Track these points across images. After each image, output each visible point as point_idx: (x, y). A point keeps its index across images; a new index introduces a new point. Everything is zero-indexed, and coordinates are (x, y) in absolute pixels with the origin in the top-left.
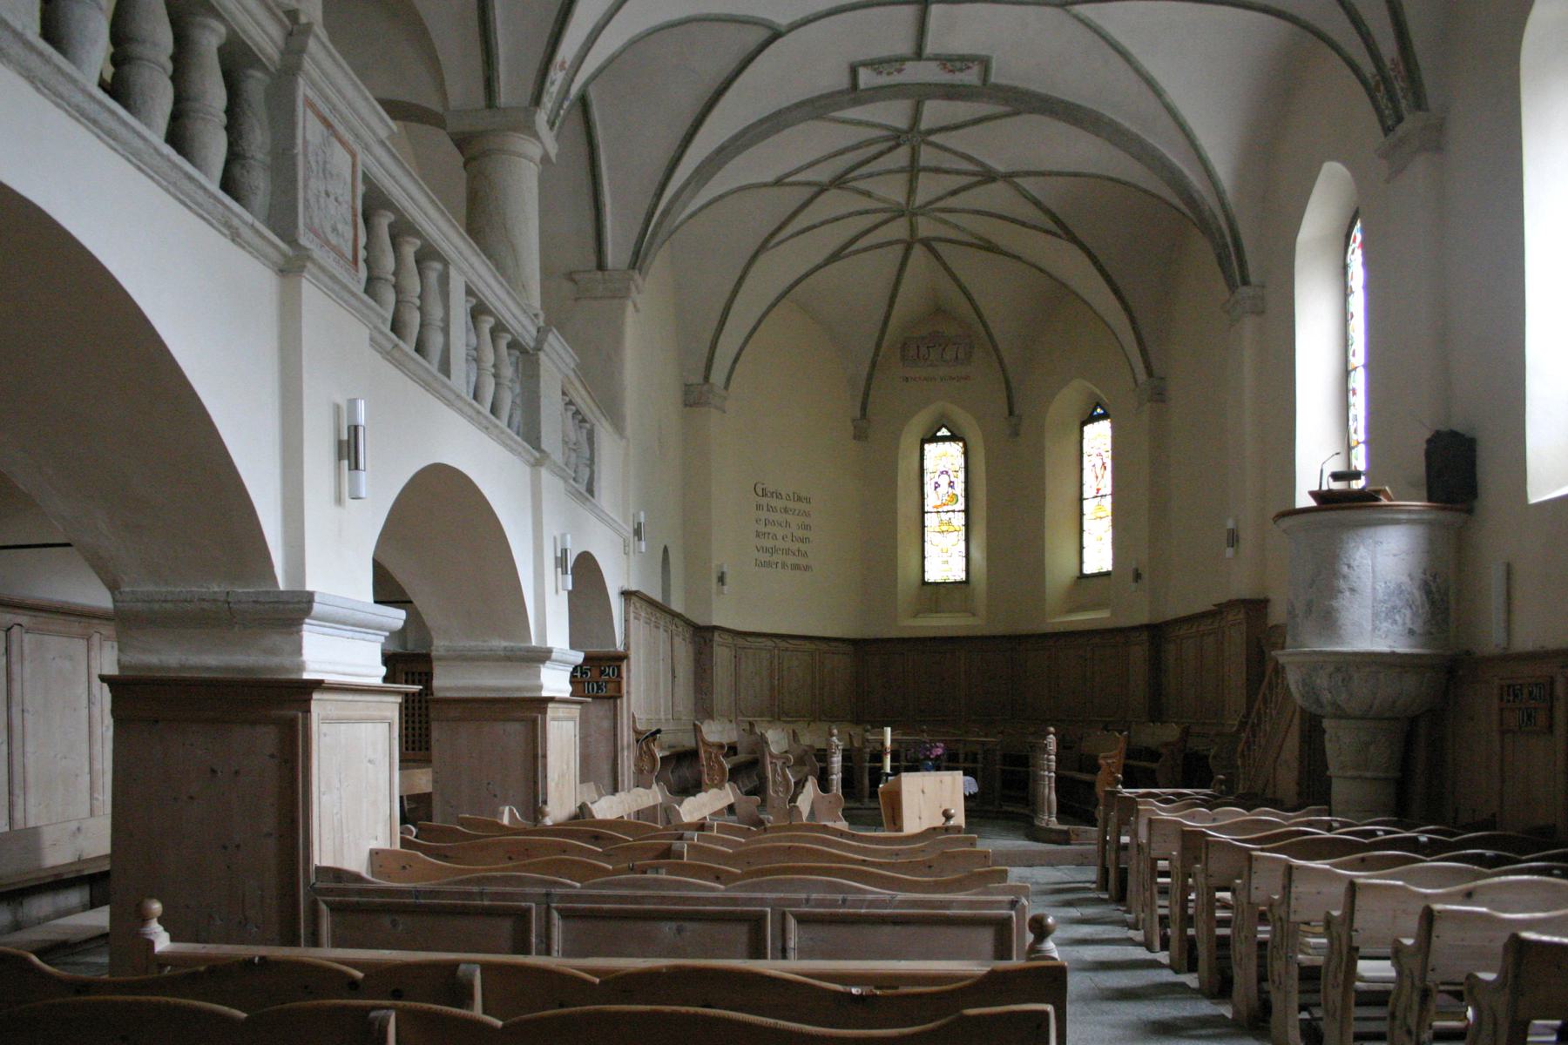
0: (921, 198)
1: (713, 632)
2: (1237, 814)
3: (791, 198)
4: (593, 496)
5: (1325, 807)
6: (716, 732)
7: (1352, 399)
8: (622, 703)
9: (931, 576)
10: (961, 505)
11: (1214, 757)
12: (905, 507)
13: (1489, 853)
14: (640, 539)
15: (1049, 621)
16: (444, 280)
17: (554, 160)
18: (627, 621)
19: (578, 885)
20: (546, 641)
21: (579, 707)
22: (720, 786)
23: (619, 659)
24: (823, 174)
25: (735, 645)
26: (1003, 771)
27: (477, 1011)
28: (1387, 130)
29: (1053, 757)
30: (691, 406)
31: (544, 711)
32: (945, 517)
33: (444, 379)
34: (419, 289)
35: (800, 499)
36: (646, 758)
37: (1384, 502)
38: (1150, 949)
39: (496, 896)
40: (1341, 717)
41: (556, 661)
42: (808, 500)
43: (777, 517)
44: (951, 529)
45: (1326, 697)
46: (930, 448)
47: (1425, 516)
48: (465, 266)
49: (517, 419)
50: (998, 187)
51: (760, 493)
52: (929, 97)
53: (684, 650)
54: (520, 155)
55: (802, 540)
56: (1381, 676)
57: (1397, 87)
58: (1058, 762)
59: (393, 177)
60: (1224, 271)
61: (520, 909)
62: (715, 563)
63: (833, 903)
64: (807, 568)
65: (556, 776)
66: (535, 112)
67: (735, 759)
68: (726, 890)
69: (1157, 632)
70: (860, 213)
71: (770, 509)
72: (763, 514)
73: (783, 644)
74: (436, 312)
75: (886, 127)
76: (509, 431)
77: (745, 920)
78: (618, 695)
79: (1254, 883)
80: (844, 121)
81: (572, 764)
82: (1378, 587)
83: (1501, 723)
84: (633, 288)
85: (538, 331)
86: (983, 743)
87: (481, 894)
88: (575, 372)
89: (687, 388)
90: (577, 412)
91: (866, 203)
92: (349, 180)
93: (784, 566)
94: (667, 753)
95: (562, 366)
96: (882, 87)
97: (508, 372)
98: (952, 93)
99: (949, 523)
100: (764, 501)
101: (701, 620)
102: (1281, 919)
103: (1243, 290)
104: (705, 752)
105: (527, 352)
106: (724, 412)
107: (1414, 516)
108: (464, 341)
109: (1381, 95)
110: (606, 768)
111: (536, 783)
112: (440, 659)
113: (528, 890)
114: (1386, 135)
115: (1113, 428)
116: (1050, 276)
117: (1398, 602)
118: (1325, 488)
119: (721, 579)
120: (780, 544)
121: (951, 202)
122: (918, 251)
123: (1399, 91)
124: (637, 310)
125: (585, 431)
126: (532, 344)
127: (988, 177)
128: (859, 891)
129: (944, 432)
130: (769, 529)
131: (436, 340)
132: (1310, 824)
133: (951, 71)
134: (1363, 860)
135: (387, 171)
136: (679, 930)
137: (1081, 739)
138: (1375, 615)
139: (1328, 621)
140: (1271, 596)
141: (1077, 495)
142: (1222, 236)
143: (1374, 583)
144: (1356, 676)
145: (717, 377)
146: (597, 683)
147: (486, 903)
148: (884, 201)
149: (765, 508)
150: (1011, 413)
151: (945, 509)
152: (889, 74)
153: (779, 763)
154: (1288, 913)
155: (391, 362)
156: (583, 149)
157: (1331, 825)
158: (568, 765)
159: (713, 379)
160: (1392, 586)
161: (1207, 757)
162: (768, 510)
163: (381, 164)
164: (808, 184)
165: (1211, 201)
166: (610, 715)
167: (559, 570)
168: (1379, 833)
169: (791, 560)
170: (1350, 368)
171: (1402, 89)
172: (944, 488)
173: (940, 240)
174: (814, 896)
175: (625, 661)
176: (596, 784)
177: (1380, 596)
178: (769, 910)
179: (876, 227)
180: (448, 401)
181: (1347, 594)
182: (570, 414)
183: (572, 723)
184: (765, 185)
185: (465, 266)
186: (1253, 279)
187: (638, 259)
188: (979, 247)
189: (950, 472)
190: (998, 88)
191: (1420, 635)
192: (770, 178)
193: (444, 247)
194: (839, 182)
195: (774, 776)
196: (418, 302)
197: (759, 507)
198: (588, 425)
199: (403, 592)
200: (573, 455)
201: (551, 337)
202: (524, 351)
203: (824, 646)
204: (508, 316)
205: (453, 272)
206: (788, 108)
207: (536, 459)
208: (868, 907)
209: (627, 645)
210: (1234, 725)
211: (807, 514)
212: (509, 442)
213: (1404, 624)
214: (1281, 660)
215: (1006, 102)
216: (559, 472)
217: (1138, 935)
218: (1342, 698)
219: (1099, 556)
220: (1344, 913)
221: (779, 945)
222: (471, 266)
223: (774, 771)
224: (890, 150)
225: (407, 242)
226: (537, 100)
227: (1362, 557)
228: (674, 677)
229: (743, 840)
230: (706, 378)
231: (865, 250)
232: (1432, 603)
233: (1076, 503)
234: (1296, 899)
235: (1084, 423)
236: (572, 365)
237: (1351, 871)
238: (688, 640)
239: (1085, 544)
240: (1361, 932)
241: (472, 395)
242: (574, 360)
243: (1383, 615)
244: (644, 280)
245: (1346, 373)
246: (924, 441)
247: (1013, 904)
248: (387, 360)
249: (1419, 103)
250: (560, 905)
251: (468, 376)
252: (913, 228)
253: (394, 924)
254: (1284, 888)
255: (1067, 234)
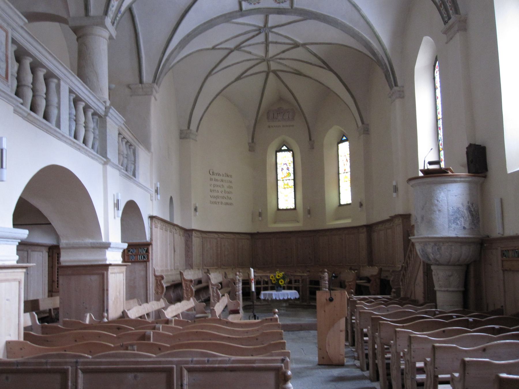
0: (271, 54)
1: (192, 232)
2: (396, 308)
3: (219, 55)
4: (135, 177)
5: (434, 304)
6: (190, 275)
7: (439, 131)
8: (149, 264)
9: (281, 207)
10: (292, 177)
11: (392, 281)
12: (270, 179)
13: (497, 327)
14: (158, 194)
15: (327, 224)
16: (58, 86)
17: (115, 37)
18: (151, 229)
19: (90, 357)
20: (109, 240)
21: (125, 267)
22: (188, 299)
23: (146, 246)
24: (231, 45)
25: (202, 237)
26: (310, 287)
27: (279, 322)
28: (445, 23)
29: (327, 282)
30: (183, 139)
31: (107, 270)
32: (286, 182)
33: (58, 130)
34: (45, 90)
35: (228, 176)
36: (160, 287)
37: (450, 173)
38: (362, 370)
39: (53, 363)
40: (438, 265)
41: (114, 248)
42: (231, 176)
43: (218, 183)
44: (288, 187)
45: (431, 256)
46: (279, 154)
47: (467, 179)
48: (68, 81)
49: (97, 145)
50: (300, 49)
51: (211, 174)
52: (271, 13)
53: (179, 239)
54: (99, 36)
55: (229, 193)
56: (453, 247)
57: (448, 5)
58: (329, 284)
59: (30, 43)
60: (388, 81)
61: (64, 369)
62: (193, 202)
63: (203, 362)
64: (231, 204)
65: (113, 299)
66: (105, 18)
67: (200, 286)
68: (156, 357)
69: (369, 228)
70: (248, 60)
71: (216, 180)
72: (213, 182)
73: (221, 236)
74: (54, 99)
75: (254, 26)
76: (92, 151)
77: (165, 371)
78: (148, 260)
79: (398, 343)
80: (238, 23)
81: (122, 293)
82: (450, 209)
83: (503, 266)
84: (154, 91)
85: (106, 108)
86: (301, 276)
87: (46, 363)
88: (124, 125)
89: (181, 132)
90: (127, 142)
91: (249, 57)
92: (4, 43)
93: (222, 203)
94: (169, 285)
95: (118, 122)
96: (251, 10)
97: (91, 125)
98: (280, 11)
99: (288, 184)
100: (213, 177)
101: (187, 227)
102: (408, 361)
103: (395, 88)
104: (185, 283)
105: (101, 117)
106: (196, 141)
107: (462, 179)
108: (68, 112)
109: (442, 8)
110: (142, 292)
111: (103, 302)
112: (64, 248)
113: (68, 360)
114: (445, 25)
115: (349, 143)
116: (323, 84)
117: (458, 215)
118: (426, 168)
119: (196, 210)
120: (220, 194)
121: (283, 56)
122: (271, 76)
123: (449, 7)
124: (156, 99)
125: (132, 150)
126: (103, 114)
127: (296, 45)
128: (215, 356)
129: (284, 148)
130: (216, 188)
131: (54, 112)
132: (426, 313)
133: (278, 3)
134: (444, 331)
135: (27, 40)
136: (135, 377)
137: (340, 273)
138: (449, 221)
139: (430, 223)
140: (411, 213)
141: (337, 171)
142: (386, 67)
143: (448, 207)
144: (443, 248)
145: (193, 127)
146: (143, 255)
147: (49, 367)
148: (256, 55)
149: (214, 180)
150: (310, 139)
151: (286, 178)
152: (254, 4)
153: (215, 288)
154: (411, 358)
155: (28, 121)
156: (133, 35)
157: (435, 313)
158: (120, 293)
159: (191, 128)
160: (455, 209)
161: (389, 281)
162: (215, 180)
163: (23, 37)
164: (226, 49)
165: (381, 53)
166: (145, 269)
167: (116, 208)
168: (454, 317)
169: (224, 201)
170: (438, 118)
171: (450, 6)
172: (285, 170)
173: (278, 70)
174: (195, 359)
175: (151, 246)
176: (137, 300)
177: (451, 213)
178: (175, 366)
179: (254, 66)
180: (59, 138)
181: (437, 212)
182: (124, 143)
183: (122, 275)
184: (208, 49)
185: (68, 81)
186: (399, 84)
187: (156, 79)
188: (296, 74)
189: (287, 164)
190: (296, 9)
191: (468, 229)
192: (210, 46)
193: (57, 72)
194: (238, 48)
195: (213, 294)
196: (45, 96)
197: (211, 179)
198: (133, 147)
199: (48, 221)
200: (125, 160)
201: (111, 111)
202: (100, 116)
203: (237, 236)
204: (90, 102)
205: (62, 83)
206: (215, 19)
207: (105, 162)
208: (219, 364)
209: (151, 239)
210: (399, 267)
211: (231, 182)
212: (91, 155)
213: (461, 225)
214: (413, 241)
215: (300, 14)
216: (114, 166)
217: (357, 363)
218: (438, 257)
219: (346, 198)
220: (431, 360)
221: (180, 383)
222: (71, 81)
223: (213, 291)
224: (257, 35)
225: (40, 70)
226: (106, 13)
227: (442, 197)
228: (175, 251)
229: (181, 328)
230: (189, 128)
231: (251, 75)
232: (472, 215)
233: (337, 175)
234: (414, 352)
235: (339, 143)
236: (122, 122)
237: (437, 338)
238: (181, 235)
239: (279, 197)
240: (438, 368)
241: (73, 135)
242: (123, 120)
243: (452, 221)
244: (159, 88)
245: (437, 120)
246: (277, 152)
247: (283, 361)
248: (26, 120)
249: (457, 11)
250: (82, 367)
251: (70, 126)
252: (269, 66)
253: (7, 378)
254: (408, 346)
255: (328, 68)
